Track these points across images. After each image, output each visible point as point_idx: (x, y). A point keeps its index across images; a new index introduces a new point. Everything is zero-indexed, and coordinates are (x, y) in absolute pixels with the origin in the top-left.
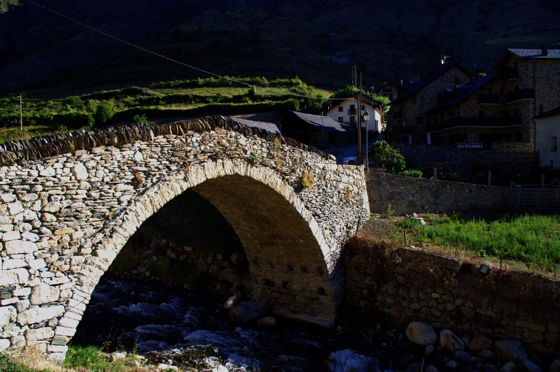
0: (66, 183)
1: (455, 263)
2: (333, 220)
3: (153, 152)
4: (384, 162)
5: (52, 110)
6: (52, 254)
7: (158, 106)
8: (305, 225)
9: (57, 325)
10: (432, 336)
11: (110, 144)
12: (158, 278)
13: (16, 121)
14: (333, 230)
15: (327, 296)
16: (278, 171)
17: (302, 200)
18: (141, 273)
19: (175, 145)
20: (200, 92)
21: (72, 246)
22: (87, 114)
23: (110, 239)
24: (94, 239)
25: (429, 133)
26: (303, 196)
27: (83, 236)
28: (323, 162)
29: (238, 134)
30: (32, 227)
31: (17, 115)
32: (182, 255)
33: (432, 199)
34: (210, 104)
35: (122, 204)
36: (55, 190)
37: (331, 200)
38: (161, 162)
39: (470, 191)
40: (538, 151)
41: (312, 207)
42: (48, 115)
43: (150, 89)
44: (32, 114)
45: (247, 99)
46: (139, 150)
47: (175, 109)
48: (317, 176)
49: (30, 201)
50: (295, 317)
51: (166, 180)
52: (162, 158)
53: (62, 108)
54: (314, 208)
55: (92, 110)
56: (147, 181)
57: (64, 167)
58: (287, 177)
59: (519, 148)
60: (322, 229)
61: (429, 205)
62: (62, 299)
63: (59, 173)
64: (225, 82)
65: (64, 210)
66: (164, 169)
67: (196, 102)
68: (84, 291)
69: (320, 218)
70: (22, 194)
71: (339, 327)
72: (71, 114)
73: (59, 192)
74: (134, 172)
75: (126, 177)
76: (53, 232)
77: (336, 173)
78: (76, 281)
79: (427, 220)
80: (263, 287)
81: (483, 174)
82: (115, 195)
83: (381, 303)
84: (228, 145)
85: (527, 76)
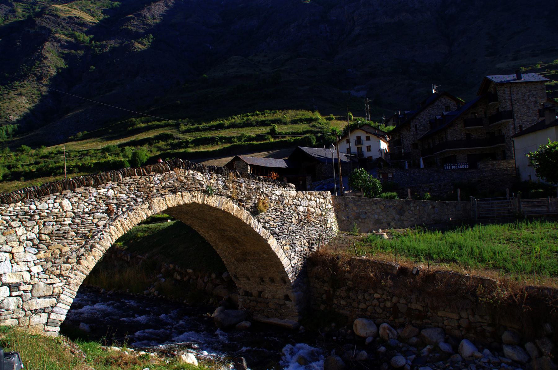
0: (56, 213)
1: (393, 267)
2: (293, 237)
3: (123, 189)
4: (361, 187)
5: (92, 158)
6: (47, 262)
7: (187, 149)
8: (264, 242)
9: (51, 312)
10: (373, 329)
11: (88, 185)
12: (164, 297)
13: (61, 170)
14: (293, 246)
15: (291, 301)
16: (233, 199)
17: (259, 221)
18: (151, 293)
19: (140, 183)
20: (226, 133)
21: (62, 257)
22: (123, 160)
23: (90, 252)
24: (78, 252)
25: (421, 158)
26: (260, 218)
27: (70, 250)
28: (280, 190)
29: (196, 172)
30: (33, 244)
31: (62, 165)
32: (185, 276)
33: (397, 217)
34: (234, 144)
35: (99, 228)
36: (48, 219)
37: (289, 220)
38: (129, 196)
39: (434, 207)
40: (518, 167)
41: (270, 227)
42: (89, 163)
43: (180, 133)
44: (75, 163)
45: (269, 136)
46: (111, 188)
47: (202, 150)
48: (274, 202)
49: (31, 226)
50: (268, 321)
51: (133, 210)
52: (129, 194)
53: (101, 156)
54: (272, 228)
55: (128, 156)
56: (118, 210)
57: (54, 202)
58: (242, 203)
59: (503, 165)
60: (282, 245)
61: (395, 222)
62: (55, 294)
63: (51, 207)
64: (250, 123)
65: (54, 232)
66: (132, 201)
67: (222, 143)
68: (71, 289)
69: (278, 236)
70: (25, 221)
71: (301, 327)
72: (109, 161)
73: (52, 220)
74: (108, 204)
75: (101, 208)
76: (48, 247)
77: (296, 198)
78: (65, 282)
79: (389, 234)
80: (243, 297)
81: (453, 192)
82: (93, 221)
83: (337, 305)
84: (185, 181)
85: (504, 99)
